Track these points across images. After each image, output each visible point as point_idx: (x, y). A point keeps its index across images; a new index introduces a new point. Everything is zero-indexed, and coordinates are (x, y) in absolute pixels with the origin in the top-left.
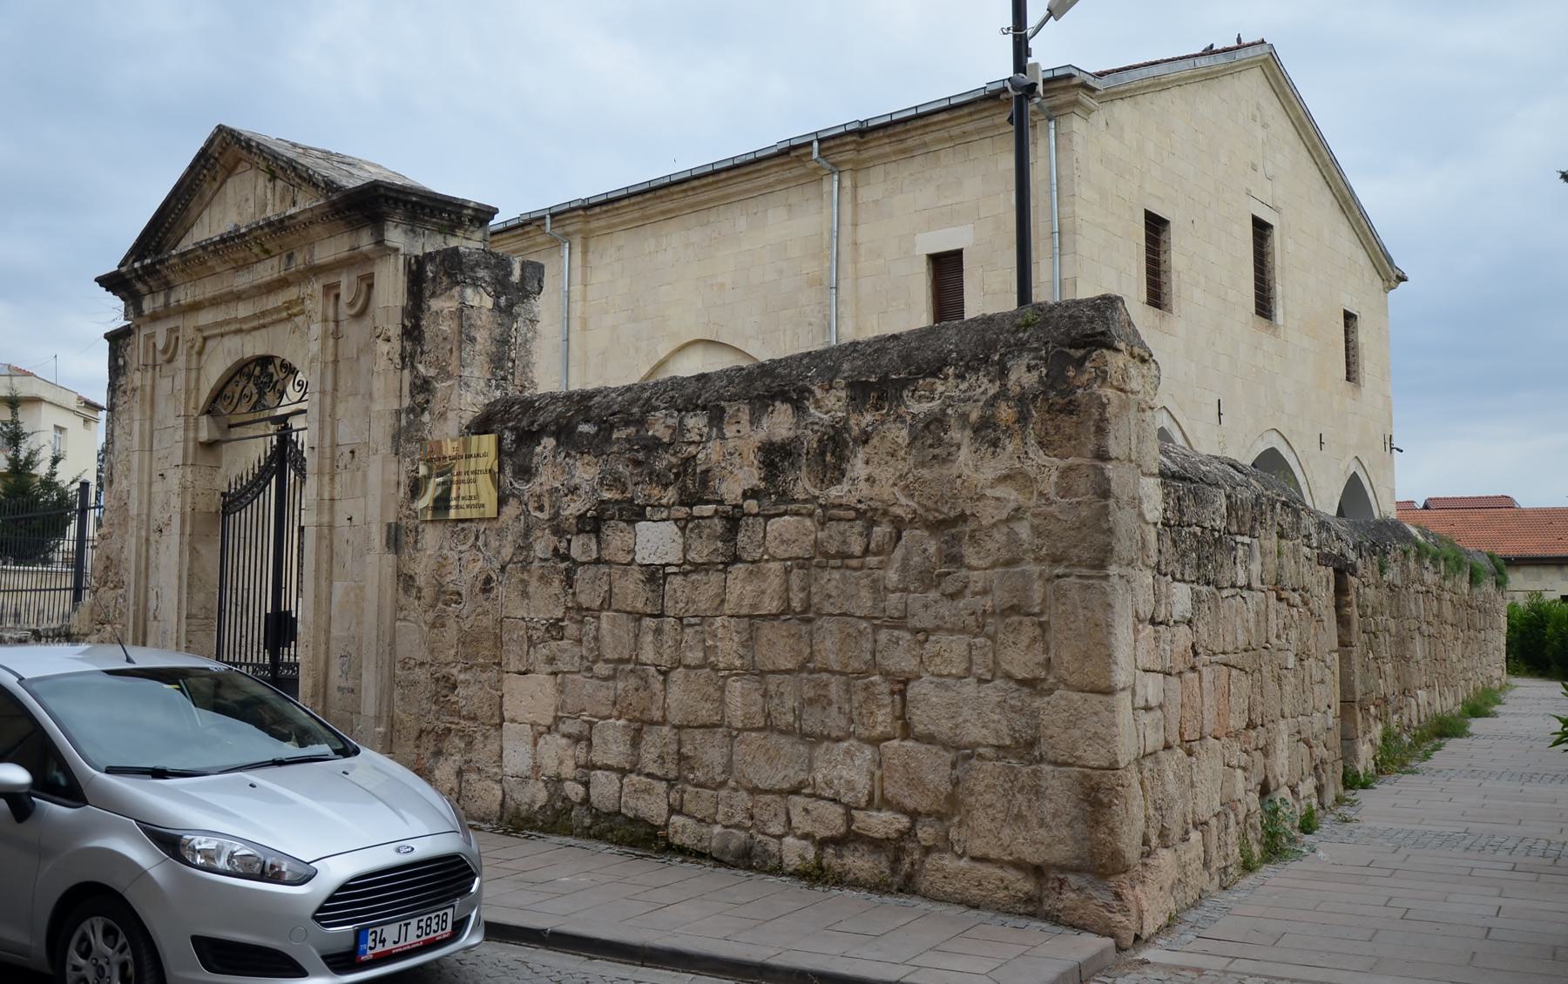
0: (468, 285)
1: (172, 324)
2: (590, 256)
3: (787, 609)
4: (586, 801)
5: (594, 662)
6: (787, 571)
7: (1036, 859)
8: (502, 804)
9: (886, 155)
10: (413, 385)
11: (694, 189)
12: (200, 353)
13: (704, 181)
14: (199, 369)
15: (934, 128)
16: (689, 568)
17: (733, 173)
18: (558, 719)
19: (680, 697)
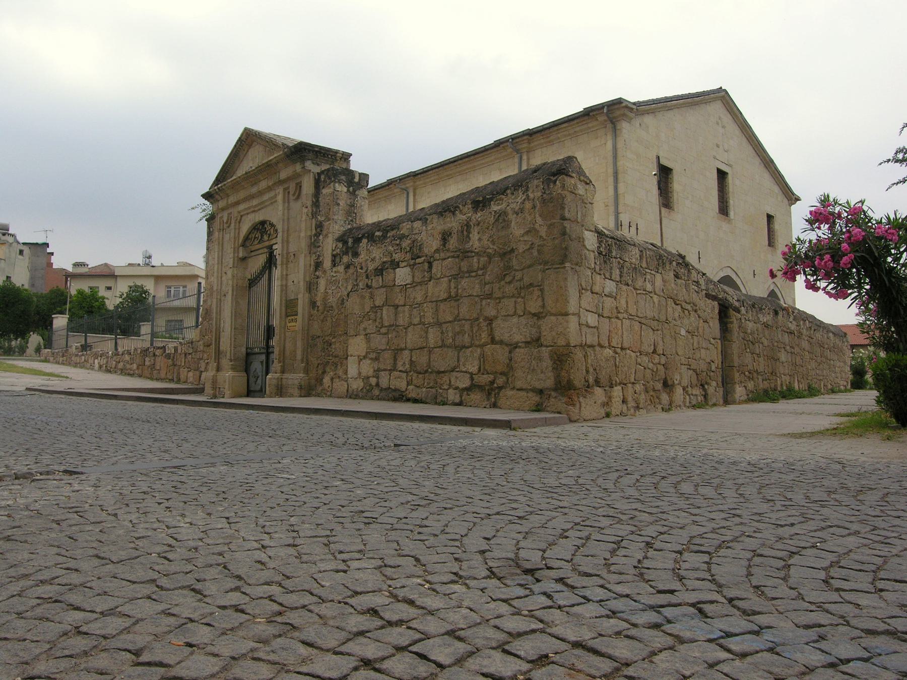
0: (336, 182)
1: (229, 211)
2: (417, 197)
3: (450, 297)
4: (377, 385)
5: (381, 328)
6: (450, 281)
7: (540, 387)
8: (348, 391)
10: (316, 224)
11: (460, 164)
12: (239, 222)
13: (464, 160)
14: (239, 229)
16: (414, 284)
17: (476, 156)
18: (367, 353)
19: (412, 338)
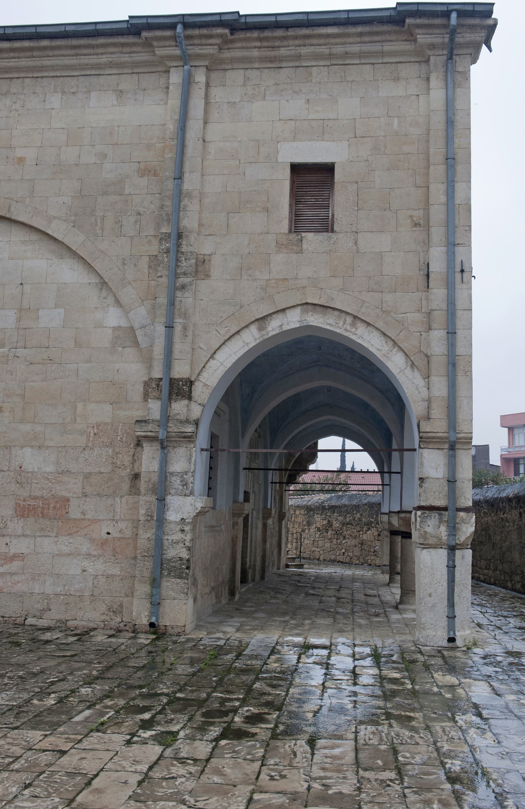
9: (249, 60)
15: (315, 41)
